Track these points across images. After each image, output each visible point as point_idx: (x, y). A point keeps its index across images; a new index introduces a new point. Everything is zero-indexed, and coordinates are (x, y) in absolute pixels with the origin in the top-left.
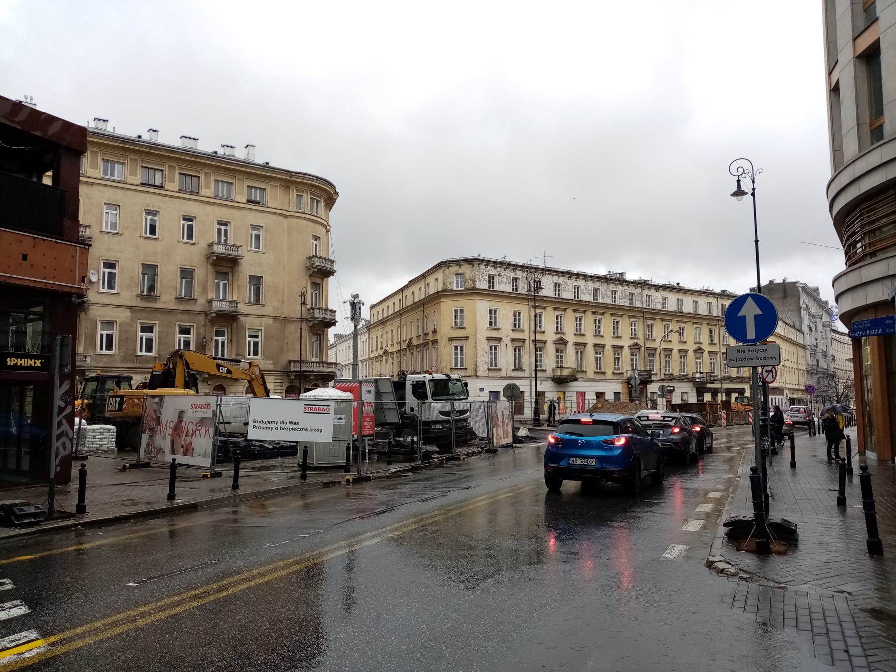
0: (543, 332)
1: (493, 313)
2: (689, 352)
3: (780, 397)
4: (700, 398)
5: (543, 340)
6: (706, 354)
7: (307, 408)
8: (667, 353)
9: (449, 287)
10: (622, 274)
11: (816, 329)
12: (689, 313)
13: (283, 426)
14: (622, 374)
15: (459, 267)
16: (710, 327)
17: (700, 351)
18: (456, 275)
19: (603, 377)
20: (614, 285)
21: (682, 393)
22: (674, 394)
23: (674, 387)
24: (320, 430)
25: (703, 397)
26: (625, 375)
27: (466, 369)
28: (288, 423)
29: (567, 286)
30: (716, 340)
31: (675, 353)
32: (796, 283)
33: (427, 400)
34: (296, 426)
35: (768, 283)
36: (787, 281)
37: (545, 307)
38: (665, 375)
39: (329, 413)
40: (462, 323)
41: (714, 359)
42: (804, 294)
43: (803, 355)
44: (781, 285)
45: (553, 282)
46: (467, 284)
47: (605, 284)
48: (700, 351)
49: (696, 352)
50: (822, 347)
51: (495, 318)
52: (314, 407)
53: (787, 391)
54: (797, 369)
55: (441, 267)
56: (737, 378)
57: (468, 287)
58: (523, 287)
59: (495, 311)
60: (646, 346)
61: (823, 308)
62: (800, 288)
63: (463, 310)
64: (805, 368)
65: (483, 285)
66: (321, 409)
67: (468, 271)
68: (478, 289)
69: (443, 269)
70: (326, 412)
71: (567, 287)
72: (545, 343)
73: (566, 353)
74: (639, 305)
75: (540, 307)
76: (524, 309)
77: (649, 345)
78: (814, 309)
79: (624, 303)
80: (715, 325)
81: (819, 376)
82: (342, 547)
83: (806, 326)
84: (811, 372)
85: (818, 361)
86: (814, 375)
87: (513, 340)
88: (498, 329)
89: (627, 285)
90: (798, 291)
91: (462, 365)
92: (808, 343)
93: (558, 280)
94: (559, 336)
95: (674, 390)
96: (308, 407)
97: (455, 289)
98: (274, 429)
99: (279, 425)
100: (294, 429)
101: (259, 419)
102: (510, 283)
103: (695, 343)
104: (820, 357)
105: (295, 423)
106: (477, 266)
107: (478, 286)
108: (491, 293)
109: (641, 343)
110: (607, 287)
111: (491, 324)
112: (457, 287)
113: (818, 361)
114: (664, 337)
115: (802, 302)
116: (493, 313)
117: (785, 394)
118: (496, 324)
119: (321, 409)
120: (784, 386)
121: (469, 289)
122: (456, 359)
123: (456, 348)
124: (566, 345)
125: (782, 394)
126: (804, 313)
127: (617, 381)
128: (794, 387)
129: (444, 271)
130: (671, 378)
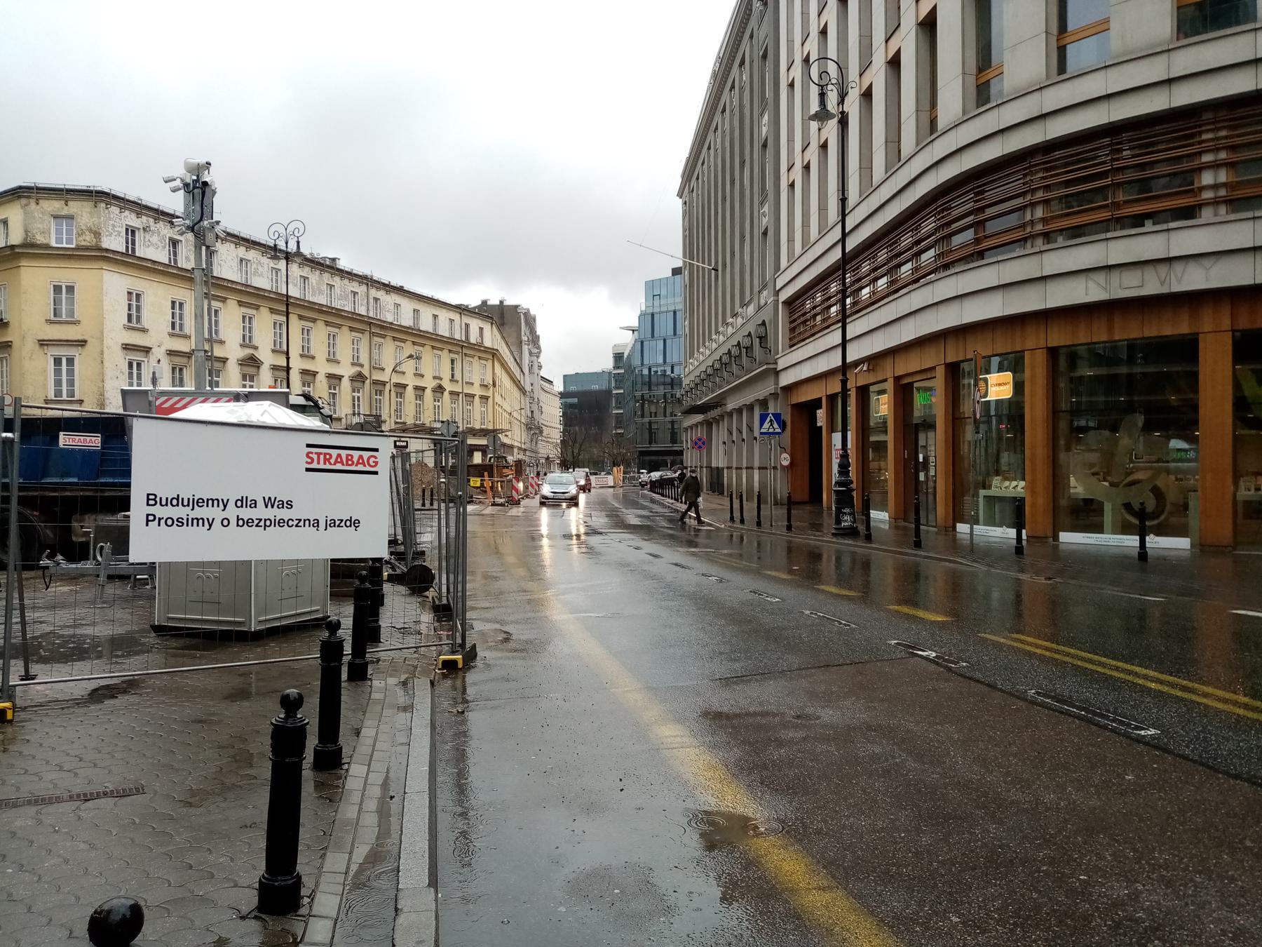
0: (222, 342)
1: (135, 298)
2: (408, 388)
5: (222, 356)
6: (446, 394)
7: (315, 457)
8: (400, 390)
9: (40, 239)
10: (334, 260)
12: (427, 332)
13: (246, 513)
15: (63, 202)
16: (453, 356)
17: (439, 389)
18: (55, 217)
23: (407, 442)
24: (355, 523)
26: (344, 421)
27: (81, 402)
28: (261, 504)
29: (259, 267)
31: (410, 391)
34: (284, 514)
36: (505, 303)
37: (226, 299)
38: (396, 423)
39: (376, 473)
40: (71, 312)
41: (439, 401)
45: (237, 256)
46: (81, 238)
47: (318, 272)
48: (439, 389)
49: (434, 391)
51: (138, 308)
52: (334, 452)
55: (20, 197)
56: (482, 430)
57: (83, 243)
58: (188, 259)
59: (138, 296)
60: (374, 378)
63: (72, 288)
65: (115, 242)
66: (355, 460)
67: (84, 214)
68: (107, 250)
69: (24, 201)
70: (368, 469)
71: (260, 269)
72: (224, 362)
73: (258, 380)
74: (364, 313)
75: (217, 298)
76: (186, 295)
77: (377, 376)
87: (171, 353)
88: (144, 331)
89: (347, 278)
91: (71, 393)
94: (249, 351)
96: (319, 454)
97: (54, 244)
98: (217, 524)
99: (232, 512)
100: (281, 523)
101: (163, 494)
102: (164, 247)
105: (282, 505)
106: (103, 205)
107: (105, 245)
108: (128, 260)
109: (366, 372)
110: (319, 277)
111: (130, 320)
112: (59, 240)
114: (396, 367)
115: (523, 333)
116: (135, 298)
118: (138, 320)
119: (355, 460)
121: (87, 249)
122: (58, 383)
123: (58, 361)
124: (258, 367)
129: (26, 205)
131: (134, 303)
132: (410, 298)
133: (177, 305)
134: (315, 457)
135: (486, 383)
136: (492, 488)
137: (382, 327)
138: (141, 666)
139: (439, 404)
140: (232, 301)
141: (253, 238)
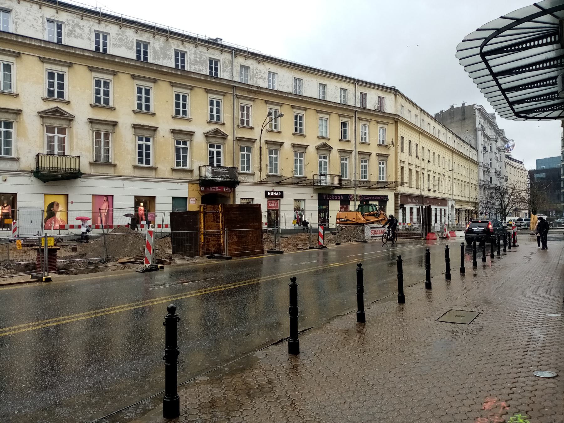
3: (443, 208)
4: (324, 207)
6: (334, 152)
11: (491, 150)
14: (191, 171)
17: (325, 148)
19: (152, 174)
20: (181, 42)
21: (44, 194)
22: (282, 201)
23: (282, 193)
25: (328, 205)
30: (350, 135)
31: (287, 148)
32: (474, 105)
33: (417, 208)
35: (450, 108)
36: (466, 105)
41: (346, 160)
42: (480, 117)
43: (476, 171)
44: (460, 109)
48: (325, 148)
50: (495, 165)
53: (454, 203)
54: (468, 183)
61: (499, 135)
62: (477, 111)
64: (477, 182)
78: (489, 132)
79: (200, 71)
80: (350, 117)
81: (491, 191)
82: (262, 279)
83: (480, 145)
84: (483, 187)
85: (491, 178)
86: (486, 190)
88: (153, 115)
90: (475, 113)
92: (481, 160)
93: (56, 15)
95: (282, 196)
103: (319, 138)
104: (493, 175)
113: (491, 178)
115: (477, 123)
117: (450, 205)
120: (450, 197)
124: (330, 151)
125: (446, 205)
126: (479, 133)
127: (179, 181)
128: (463, 199)
130: (278, 180)
131: (245, 113)
132: (289, 68)
133: (245, 108)
134: (372, 231)
135: (385, 144)
136: (247, 246)
137: (250, 91)
138: (138, 400)
139: (384, 166)
140: (260, 101)
141: (124, 17)
